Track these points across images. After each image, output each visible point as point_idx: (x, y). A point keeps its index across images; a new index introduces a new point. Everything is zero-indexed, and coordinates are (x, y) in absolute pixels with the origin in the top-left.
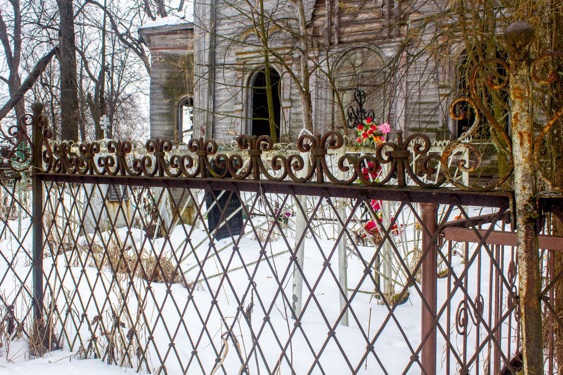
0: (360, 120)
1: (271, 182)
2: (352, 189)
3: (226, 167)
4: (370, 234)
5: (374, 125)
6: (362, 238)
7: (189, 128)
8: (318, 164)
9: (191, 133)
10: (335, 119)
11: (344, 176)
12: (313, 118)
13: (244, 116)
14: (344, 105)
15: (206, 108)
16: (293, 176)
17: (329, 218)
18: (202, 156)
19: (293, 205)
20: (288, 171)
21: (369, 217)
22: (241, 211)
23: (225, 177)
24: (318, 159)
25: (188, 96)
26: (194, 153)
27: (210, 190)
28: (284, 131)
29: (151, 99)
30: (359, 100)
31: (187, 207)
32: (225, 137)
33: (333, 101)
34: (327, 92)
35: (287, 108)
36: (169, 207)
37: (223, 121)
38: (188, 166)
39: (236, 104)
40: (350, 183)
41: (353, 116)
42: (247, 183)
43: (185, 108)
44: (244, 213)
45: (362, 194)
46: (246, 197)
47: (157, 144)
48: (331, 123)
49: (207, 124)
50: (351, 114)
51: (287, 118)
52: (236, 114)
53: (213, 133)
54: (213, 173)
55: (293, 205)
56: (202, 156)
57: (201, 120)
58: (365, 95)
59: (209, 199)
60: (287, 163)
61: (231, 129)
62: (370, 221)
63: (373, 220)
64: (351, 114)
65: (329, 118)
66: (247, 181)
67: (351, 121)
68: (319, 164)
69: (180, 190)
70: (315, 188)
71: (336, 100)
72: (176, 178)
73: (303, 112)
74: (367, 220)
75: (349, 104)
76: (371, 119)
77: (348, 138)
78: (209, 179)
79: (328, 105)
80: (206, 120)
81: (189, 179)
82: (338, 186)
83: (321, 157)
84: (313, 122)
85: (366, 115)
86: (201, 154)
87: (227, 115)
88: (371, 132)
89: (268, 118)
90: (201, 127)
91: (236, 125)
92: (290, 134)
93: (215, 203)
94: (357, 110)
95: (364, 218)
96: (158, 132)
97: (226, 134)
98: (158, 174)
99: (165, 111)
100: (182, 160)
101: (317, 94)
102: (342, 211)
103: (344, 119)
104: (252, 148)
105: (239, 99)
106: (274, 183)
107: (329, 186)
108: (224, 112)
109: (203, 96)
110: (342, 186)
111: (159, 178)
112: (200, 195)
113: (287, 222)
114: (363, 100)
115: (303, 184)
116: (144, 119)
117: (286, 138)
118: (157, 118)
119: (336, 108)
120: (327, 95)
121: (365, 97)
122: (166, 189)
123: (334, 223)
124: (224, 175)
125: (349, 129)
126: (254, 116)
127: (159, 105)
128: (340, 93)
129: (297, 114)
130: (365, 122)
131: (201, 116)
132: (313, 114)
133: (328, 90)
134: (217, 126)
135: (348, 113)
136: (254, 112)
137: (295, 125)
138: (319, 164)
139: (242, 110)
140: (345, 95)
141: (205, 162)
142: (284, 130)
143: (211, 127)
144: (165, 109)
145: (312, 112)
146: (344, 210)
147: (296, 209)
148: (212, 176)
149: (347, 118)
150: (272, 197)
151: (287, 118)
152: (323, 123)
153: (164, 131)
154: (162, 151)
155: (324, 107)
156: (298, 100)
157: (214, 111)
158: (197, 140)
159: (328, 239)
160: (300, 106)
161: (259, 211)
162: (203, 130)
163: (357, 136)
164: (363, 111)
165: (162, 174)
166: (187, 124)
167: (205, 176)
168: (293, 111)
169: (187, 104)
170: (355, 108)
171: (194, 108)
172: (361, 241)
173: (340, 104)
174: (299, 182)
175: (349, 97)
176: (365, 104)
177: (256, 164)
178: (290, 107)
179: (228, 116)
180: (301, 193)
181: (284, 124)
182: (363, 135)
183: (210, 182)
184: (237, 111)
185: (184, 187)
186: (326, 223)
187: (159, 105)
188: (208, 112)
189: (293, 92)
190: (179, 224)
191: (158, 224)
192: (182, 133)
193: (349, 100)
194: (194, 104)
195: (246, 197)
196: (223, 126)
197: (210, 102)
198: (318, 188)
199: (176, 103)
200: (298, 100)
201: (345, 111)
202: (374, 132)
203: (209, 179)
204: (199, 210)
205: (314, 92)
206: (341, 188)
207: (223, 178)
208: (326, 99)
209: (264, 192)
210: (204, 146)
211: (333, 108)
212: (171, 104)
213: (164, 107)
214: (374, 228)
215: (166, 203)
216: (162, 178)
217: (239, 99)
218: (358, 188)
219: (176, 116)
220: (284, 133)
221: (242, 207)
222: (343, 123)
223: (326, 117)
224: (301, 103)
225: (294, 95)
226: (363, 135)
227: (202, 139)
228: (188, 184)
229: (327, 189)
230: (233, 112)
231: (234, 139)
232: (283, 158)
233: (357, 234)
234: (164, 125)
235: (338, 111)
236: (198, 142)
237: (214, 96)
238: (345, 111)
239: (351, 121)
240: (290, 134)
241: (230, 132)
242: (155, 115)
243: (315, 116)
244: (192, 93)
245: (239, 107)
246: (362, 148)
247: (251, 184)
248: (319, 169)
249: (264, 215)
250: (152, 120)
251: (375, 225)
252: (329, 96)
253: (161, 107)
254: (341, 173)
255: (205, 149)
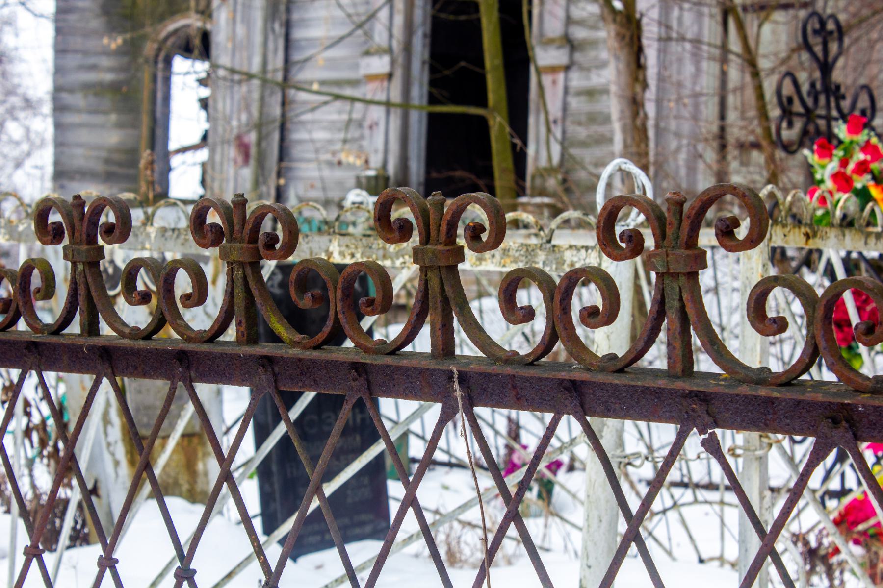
0: (822, 123)
1: (497, 368)
2: (798, 403)
3: (327, 301)
4: (857, 542)
5: (874, 140)
6: (825, 559)
7: (196, 139)
8: (673, 304)
9: (203, 155)
10: (732, 116)
11: (764, 353)
12: (650, 109)
13: (396, 96)
14: (764, 64)
15: (255, 66)
16: (577, 347)
17: (706, 480)
18: (242, 265)
19: (573, 441)
20: (560, 327)
21: (851, 481)
22: (380, 457)
23: (326, 342)
24: (672, 287)
25: (193, 21)
26: (211, 252)
27: (270, 390)
28: (544, 154)
29: (58, 31)
30: (818, 49)
31: (184, 436)
32: (327, 173)
33: (724, 48)
34: (700, 15)
35: (553, 69)
36: (116, 432)
37: (318, 115)
38: (186, 298)
39: (367, 53)
40: (789, 379)
41: (797, 107)
42: (407, 369)
43: (180, 64)
44: (389, 461)
45: (835, 422)
46: (403, 414)
47: (75, 214)
48: (715, 128)
49: (260, 126)
50: (790, 100)
51: (554, 107)
52: (369, 91)
53: (281, 159)
54: (280, 329)
55: (573, 441)
56: (242, 265)
57: (239, 110)
58: (841, 32)
59: (261, 420)
60: (557, 298)
61: (351, 143)
62: (857, 494)
63: (865, 493)
64: (790, 100)
65: (710, 110)
66: (405, 362)
67: (790, 125)
68: (676, 304)
69: (157, 387)
70: (658, 393)
71: (735, 45)
72: (141, 344)
73: (613, 88)
74: (844, 492)
75: (784, 62)
76: (862, 121)
77: (779, 195)
78: (265, 349)
79: (705, 65)
80: (255, 113)
81: (190, 347)
82: (745, 390)
83: (683, 279)
84: (651, 123)
85: (846, 104)
86: (235, 257)
87: (335, 92)
88: (862, 168)
89: (483, 103)
90: (239, 138)
91: (367, 132)
92: (565, 169)
93: (281, 429)
94: (813, 85)
95: (834, 484)
96: (79, 151)
97: (330, 164)
98: (75, 328)
99: (109, 77)
100: (165, 275)
101: (665, 24)
102: (756, 464)
103: (763, 114)
104: (426, 239)
105: (380, 37)
106: (509, 370)
107: (711, 387)
108: (322, 83)
109: (248, 22)
110: (763, 392)
111: (81, 341)
112: (232, 402)
113: (550, 492)
114: (834, 47)
115: (616, 380)
116: (29, 104)
117: (552, 183)
118: (77, 100)
119: (734, 74)
120: (700, 28)
121: (841, 40)
122: (105, 381)
123: (722, 503)
124: (320, 337)
125: (780, 154)
126: (433, 100)
127: (85, 53)
128: (751, 22)
129: (590, 93)
130: (841, 130)
131: (237, 97)
132: (650, 94)
133: (706, 10)
134: (297, 135)
135: (779, 92)
136: (432, 83)
137: (582, 133)
138: (677, 306)
139: (390, 76)
140: (767, 28)
141: (252, 285)
142: (541, 151)
143: (272, 145)
144: (111, 70)
145: (645, 86)
146: (762, 461)
147: (583, 450)
148: (276, 339)
149: (775, 112)
150: (494, 419)
151: (554, 107)
152: (686, 127)
153: (98, 148)
154: (92, 240)
155: (689, 68)
156: (593, 44)
157: (286, 78)
158: (224, 203)
159: (701, 561)
160: (603, 65)
161: (448, 452)
162: (244, 149)
163: (812, 182)
164: (834, 92)
165: (91, 328)
166: (186, 122)
167: (250, 336)
168: (577, 80)
169: (187, 50)
170: (803, 77)
171: (215, 67)
172: (820, 568)
173: (750, 61)
174: (602, 370)
175: (784, 38)
176: (840, 62)
177: (442, 297)
178: (567, 68)
179: (338, 97)
180: (608, 412)
181: (543, 130)
182: (836, 177)
183: (268, 361)
184: (371, 78)
185: (170, 376)
186: (696, 501)
187: (85, 53)
188: (265, 82)
189: (577, 12)
190: (150, 497)
191: (73, 494)
192: (167, 156)
193: (783, 47)
194: (214, 52)
195: (403, 414)
196: (320, 135)
197: (271, 45)
198: (672, 392)
199: (149, 48)
200: (593, 44)
201: (769, 86)
202: (875, 166)
203: (265, 349)
204: (225, 462)
205: (655, 14)
206: (756, 397)
207: (317, 347)
208: (697, 42)
209: (470, 403)
210: (248, 227)
211: (724, 74)
212: (132, 49)
213: (105, 62)
214: (872, 522)
215: (106, 420)
216: (93, 341)
217: (380, 37)
218: (820, 398)
219: (145, 95)
220: (543, 162)
221: (379, 447)
222: (759, 131)
223: (696, 106)
224: (604, 55)
225: (581, 23)
226: (836, 177)
227: (241, 202)
228: (188, 368)
229: (704, 398)
230: (354, 83)
231: (359, 185)
232: (544, 282)
233: (806, 543)
234: (102, 126)
235: (742, 88)
236: (227, 212)
237: (288, 26)
238: (769, 86)
239: (790, 125)
240: (565, 169)
241: (343, 157)
242: (71, 91)
243: (659, 102)
244: (206, 12)
245: (380, 65)
246: (832, 233)
247: (422, 372)
248: (677, 325)
249: (460, 466)
250: (59, 108)
251: (874, 514)
252: (710, 29)
253: (92, 60)
254: (753, 337)
255: (253, 238)
